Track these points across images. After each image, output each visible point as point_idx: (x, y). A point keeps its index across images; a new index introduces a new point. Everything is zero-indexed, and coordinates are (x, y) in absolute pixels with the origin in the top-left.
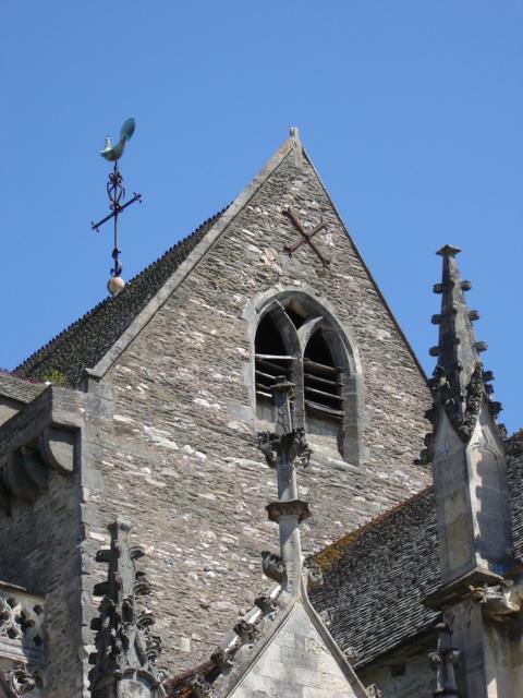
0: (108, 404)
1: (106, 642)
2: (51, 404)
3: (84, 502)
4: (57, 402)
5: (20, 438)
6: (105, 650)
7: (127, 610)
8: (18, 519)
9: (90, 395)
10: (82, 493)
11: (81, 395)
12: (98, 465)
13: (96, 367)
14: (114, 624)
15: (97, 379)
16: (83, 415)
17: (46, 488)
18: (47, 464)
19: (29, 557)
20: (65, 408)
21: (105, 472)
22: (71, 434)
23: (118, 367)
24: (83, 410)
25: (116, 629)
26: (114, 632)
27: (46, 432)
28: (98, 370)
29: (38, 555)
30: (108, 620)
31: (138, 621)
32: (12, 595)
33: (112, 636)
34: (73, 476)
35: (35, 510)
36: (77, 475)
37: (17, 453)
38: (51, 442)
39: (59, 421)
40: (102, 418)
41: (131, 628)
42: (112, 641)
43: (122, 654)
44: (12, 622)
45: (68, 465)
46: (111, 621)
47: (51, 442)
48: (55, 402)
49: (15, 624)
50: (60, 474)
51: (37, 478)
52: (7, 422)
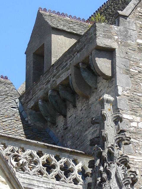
0: (133, 33)
1: (97, 175)
2: (95, 34)
3: (119, 95)
4: (100, 33)
5: (78, 58)
6: (96, 180)
7: (110, 154)
8: (80, 109)
9: (121, 28)
10: (117, 90)
11: (115, 28)
12: (127, 72)
13: (125, 10)
14: (102, 163)
15: (125, 17)
16: (117, 41)
17: (96, 88)
18: (95, 73)
19: (87, 132)
20: (105, 36)
21: (132, 76)
22: (109, 53)
23: (139, 9)
24: (116, 37)
25: (103, 166)
26: (102, 169)
27: (93, 52)
28: (125, 12)
29: (92, 131)
30: (98, 161)
31: (118, 161)
32: (75, 157)
33: (101, 172)
34: (111, 79)
35: (90, 102)
36: (113, 79)
37: (77, 67)
38: (97, 59)
39: (101, 45)
40: (129, 42)
41: (113, 165)
42: (101, 174)
43: (107, 182)
44: (75, 174)
45: (109, 73)
46: (100, 162)
47: (97, 59)
48: (98, 33)
49: (78, 175)
50: (104, 78)
51: (90, 83)
52: (70, 48)
